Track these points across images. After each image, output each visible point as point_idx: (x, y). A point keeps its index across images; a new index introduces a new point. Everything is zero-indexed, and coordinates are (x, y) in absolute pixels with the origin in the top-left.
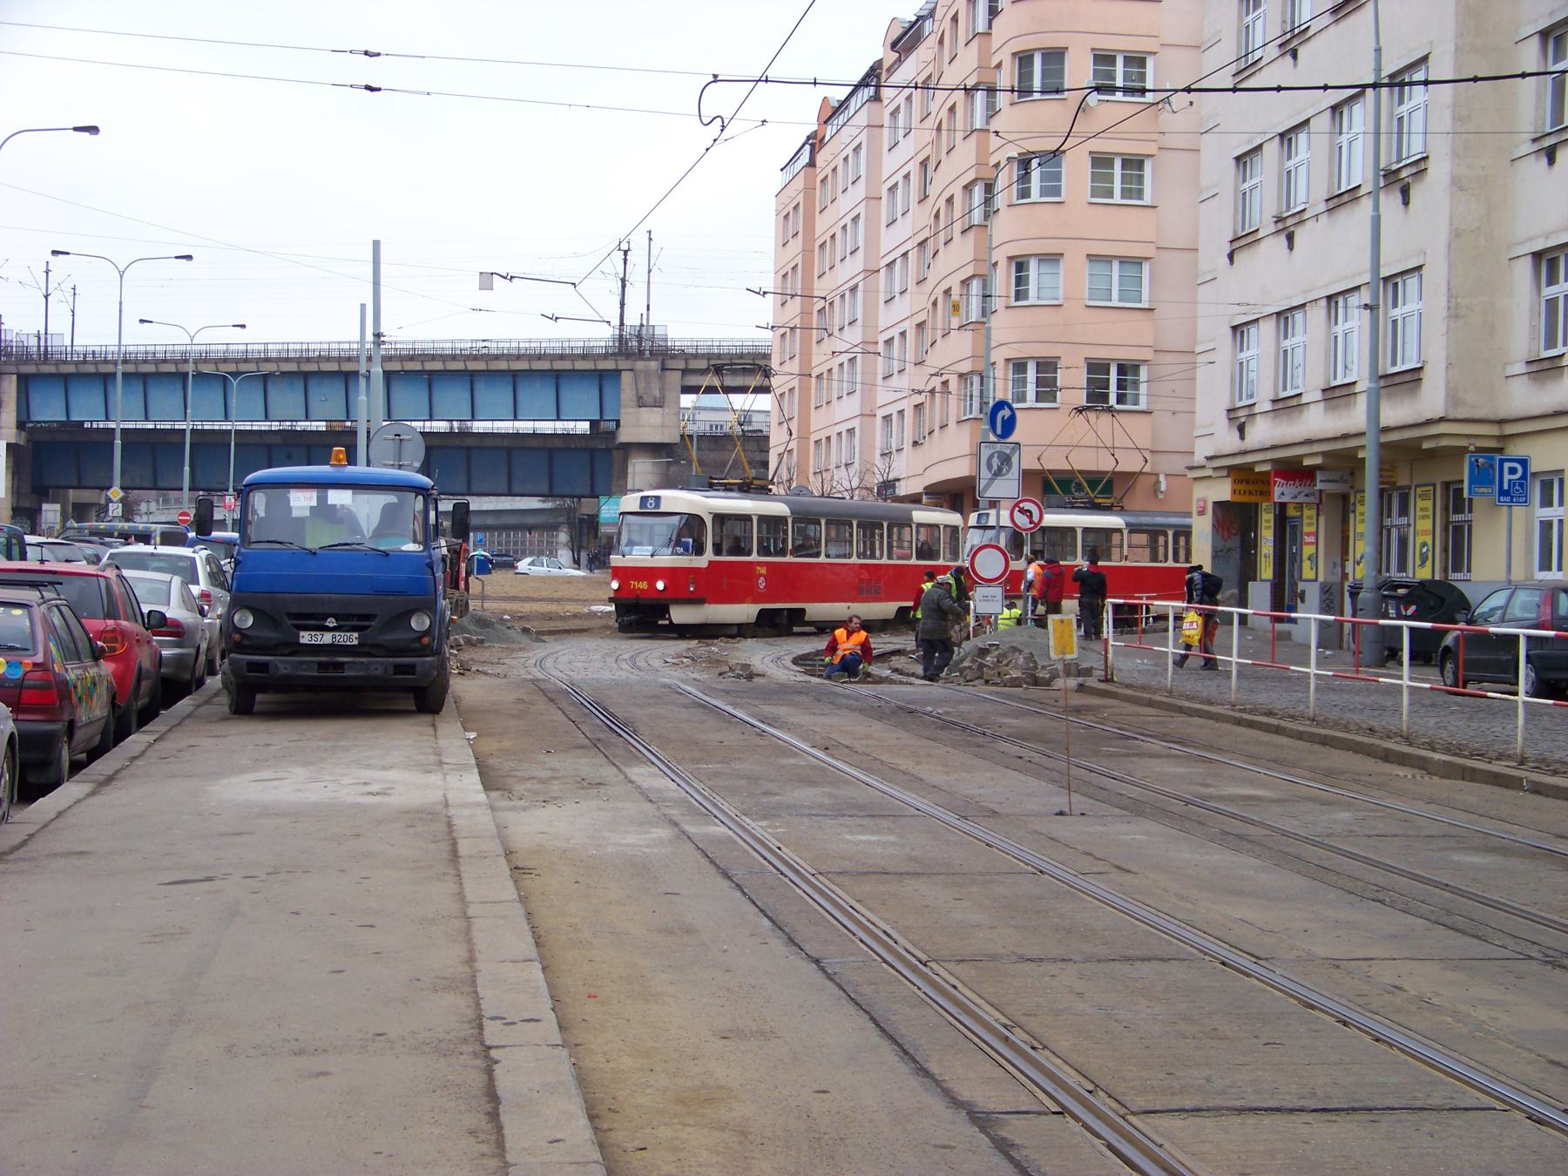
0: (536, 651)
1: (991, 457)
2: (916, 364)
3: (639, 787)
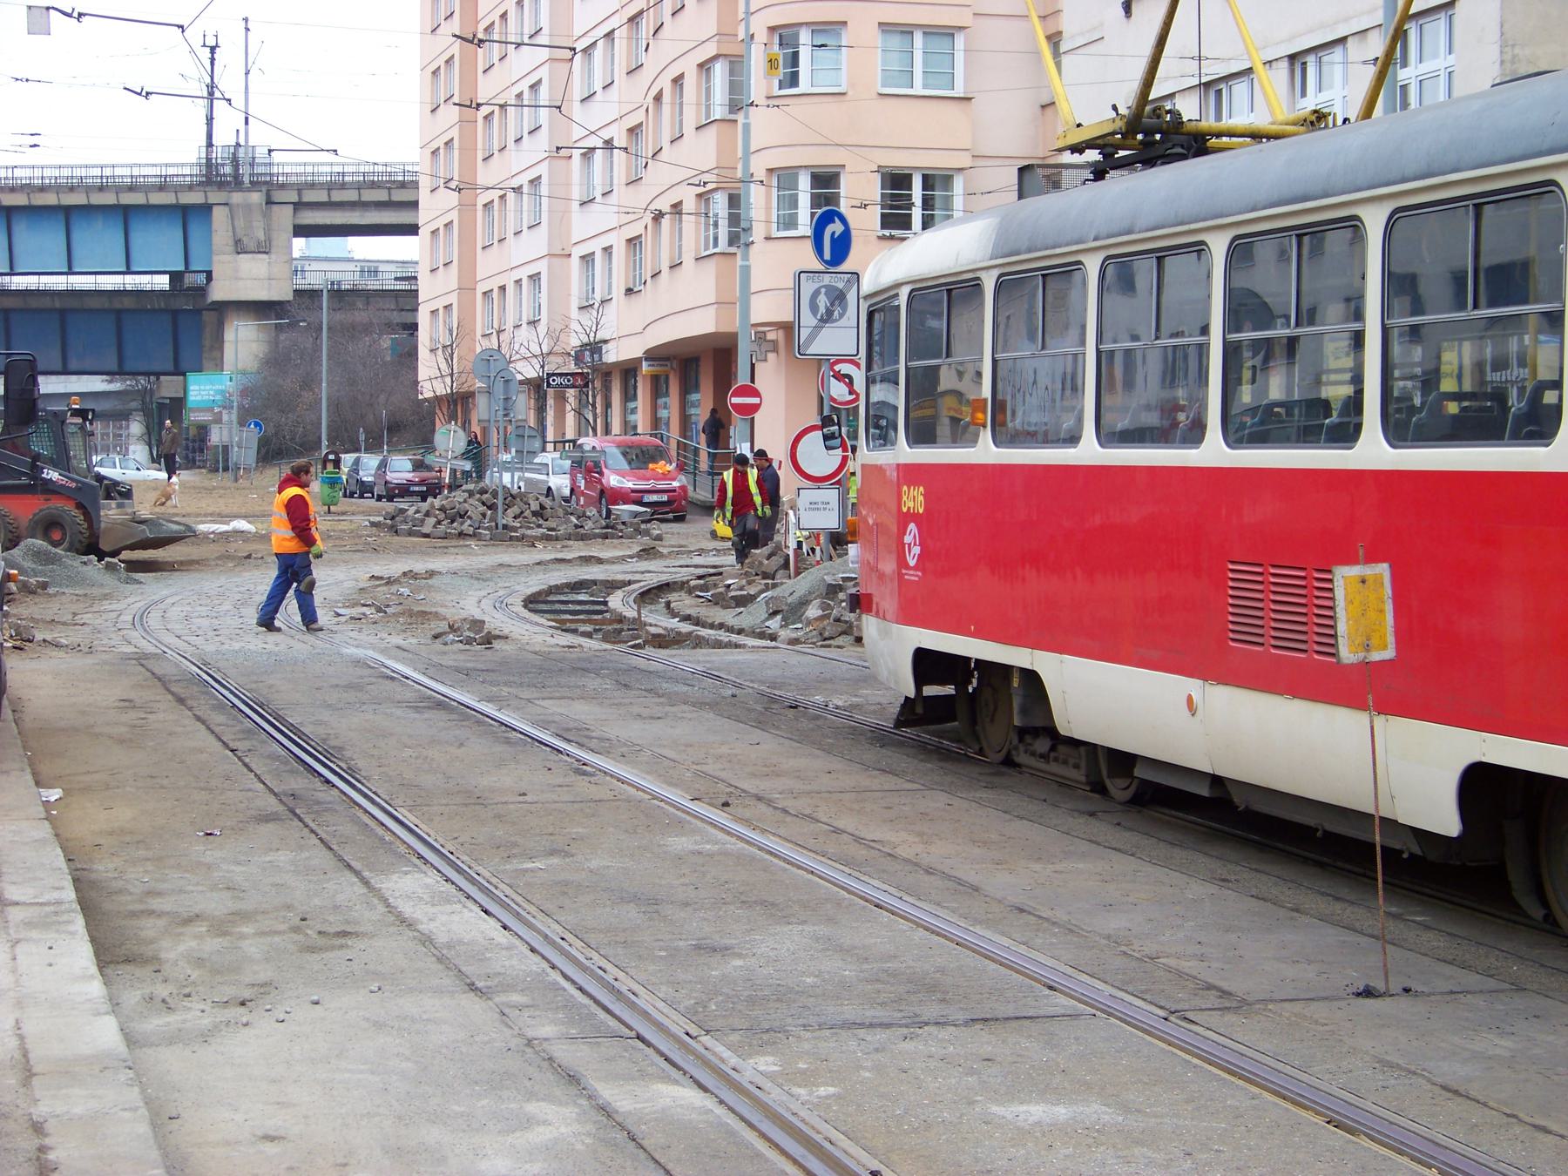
0: (131, 600)
1: (816, 293)
2: (627, 184)
3: (427, 940)
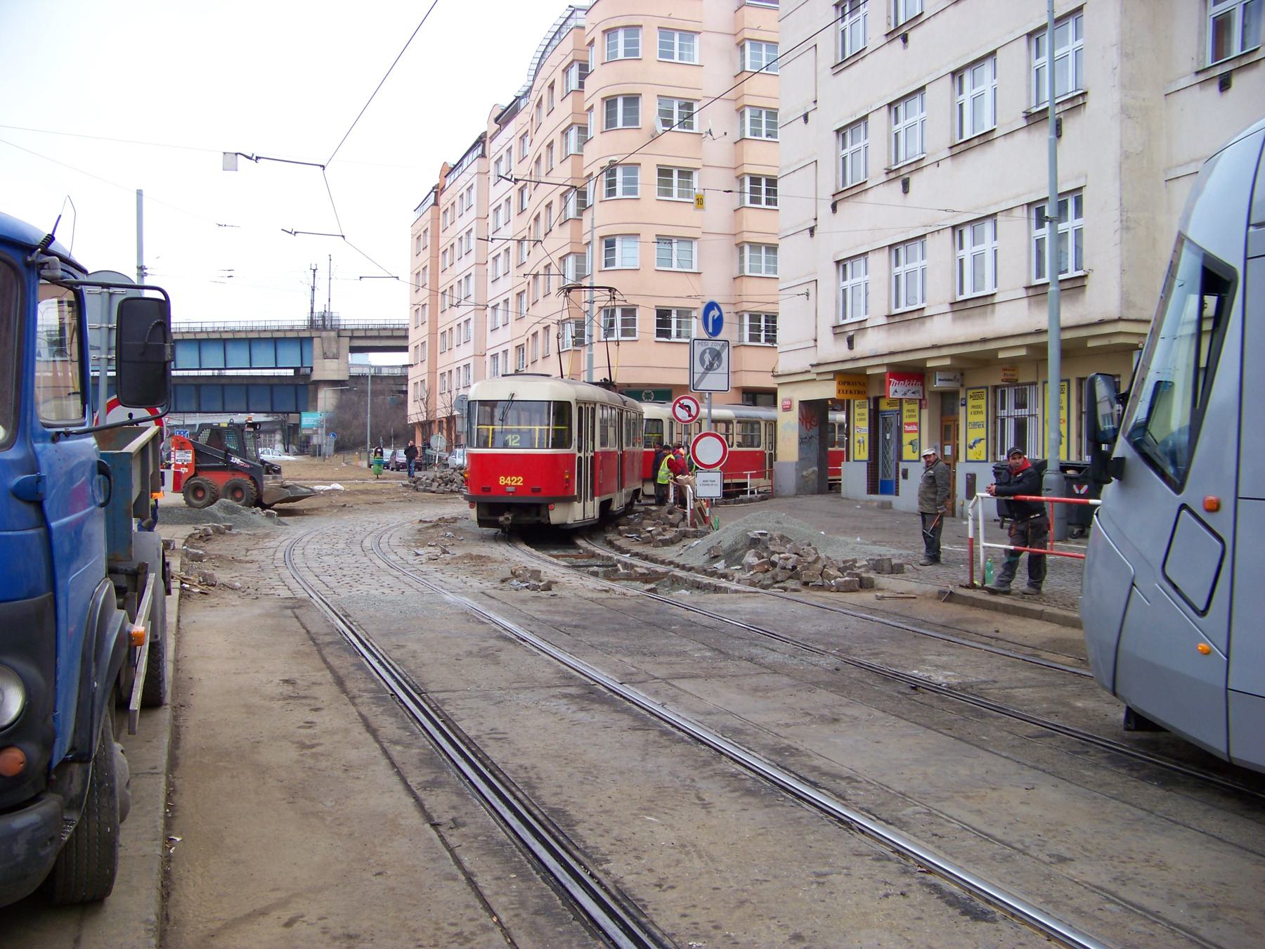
0: (282, 538)
1: (704, 353)
